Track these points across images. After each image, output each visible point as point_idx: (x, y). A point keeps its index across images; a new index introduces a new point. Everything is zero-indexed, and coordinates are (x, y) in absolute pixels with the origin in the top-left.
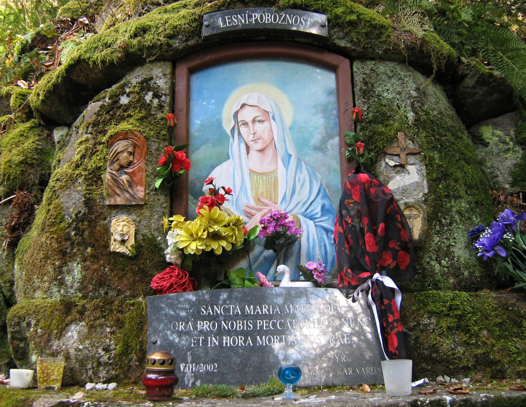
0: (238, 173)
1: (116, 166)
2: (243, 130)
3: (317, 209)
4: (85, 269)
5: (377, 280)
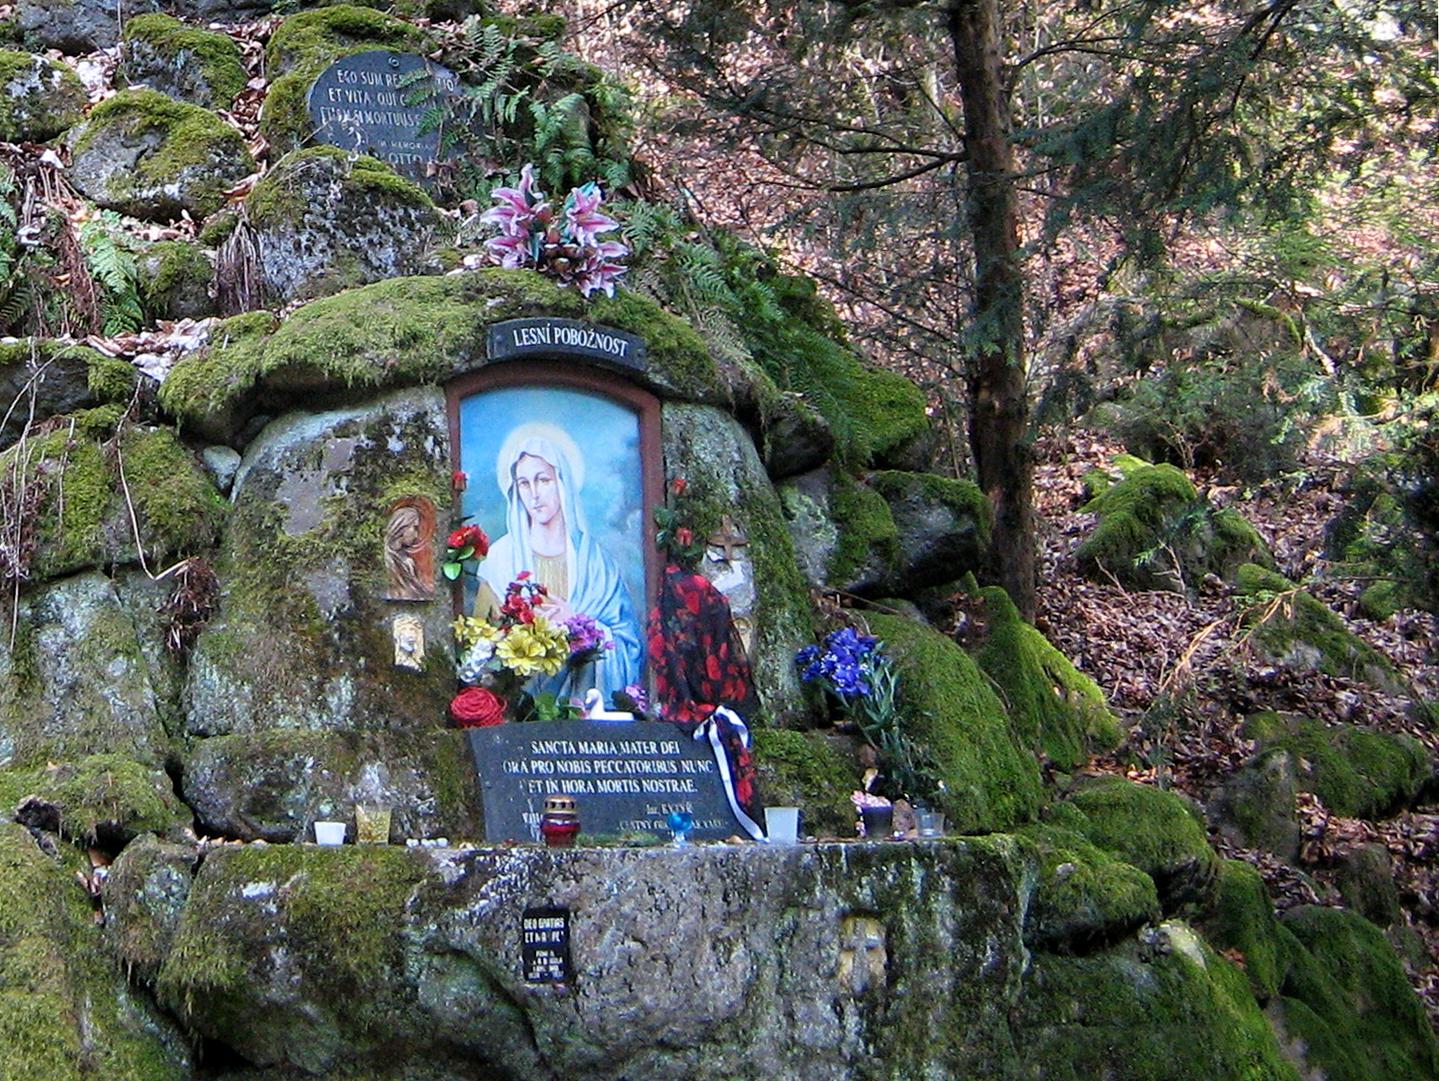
0: (518, 554)
1: (398, 545)
2: (523, 490)
3: (614, 612)
4: (358, 687)
5: (722, 715)
